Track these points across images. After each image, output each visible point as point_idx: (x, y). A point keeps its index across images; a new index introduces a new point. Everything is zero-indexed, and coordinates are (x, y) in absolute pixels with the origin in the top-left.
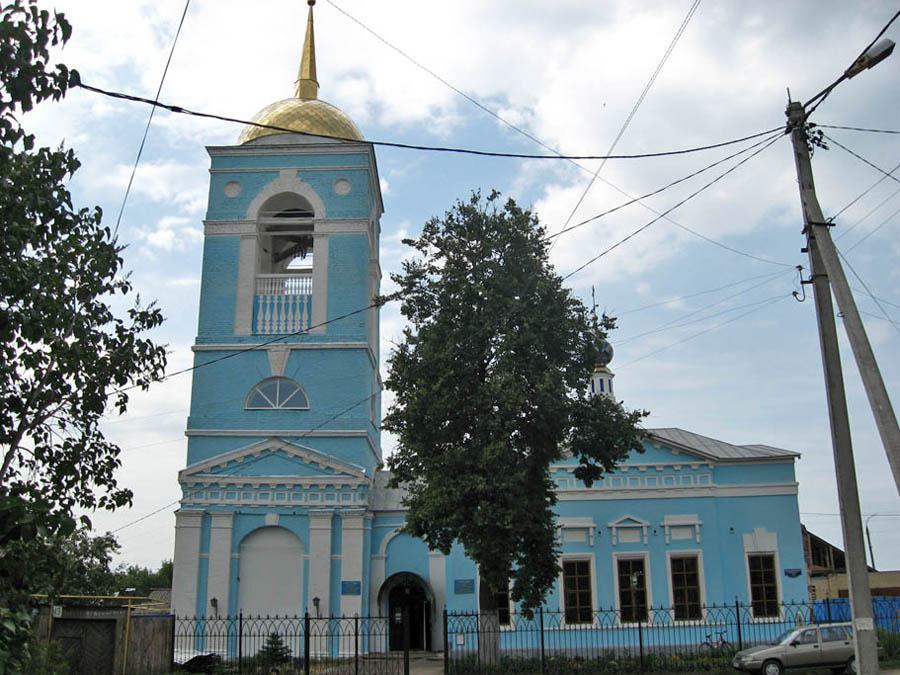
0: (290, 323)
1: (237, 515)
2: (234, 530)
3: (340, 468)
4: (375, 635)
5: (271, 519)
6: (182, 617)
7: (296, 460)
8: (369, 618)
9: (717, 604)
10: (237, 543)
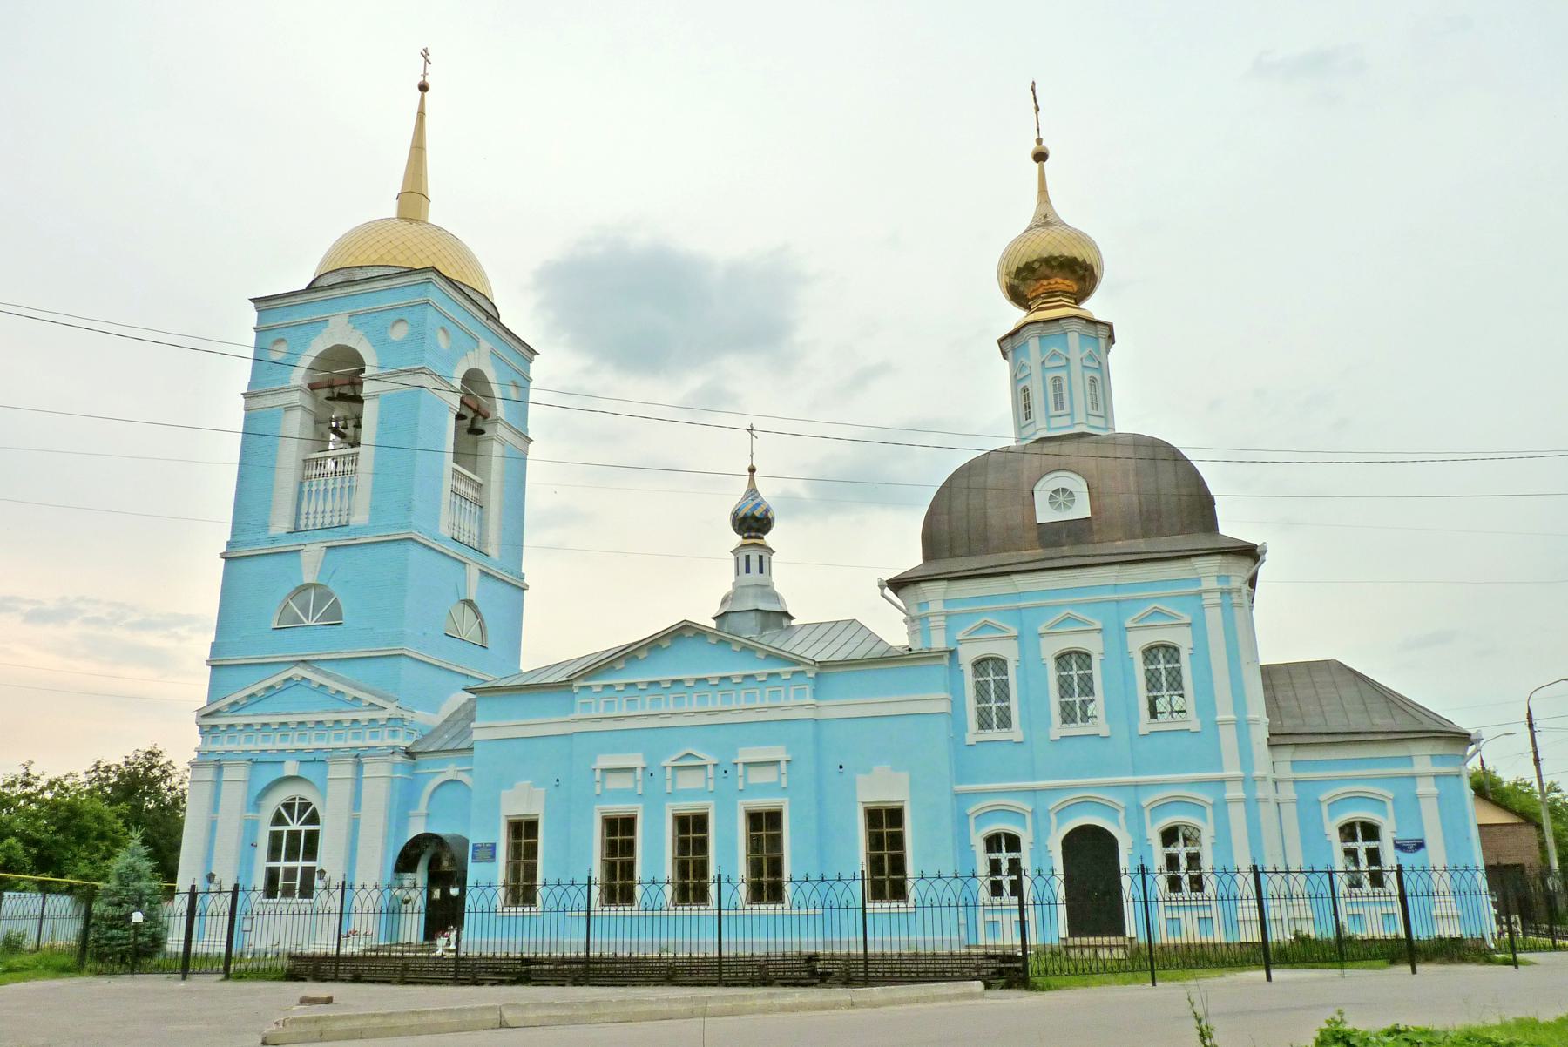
0: (319, 515)
1: (254, 762)
2: (250, 783)
3: (367, 698)
4: (406, 913)
5: (290, 768)
7: (321, 689)
9: (944, 874)
10: (253, 800)
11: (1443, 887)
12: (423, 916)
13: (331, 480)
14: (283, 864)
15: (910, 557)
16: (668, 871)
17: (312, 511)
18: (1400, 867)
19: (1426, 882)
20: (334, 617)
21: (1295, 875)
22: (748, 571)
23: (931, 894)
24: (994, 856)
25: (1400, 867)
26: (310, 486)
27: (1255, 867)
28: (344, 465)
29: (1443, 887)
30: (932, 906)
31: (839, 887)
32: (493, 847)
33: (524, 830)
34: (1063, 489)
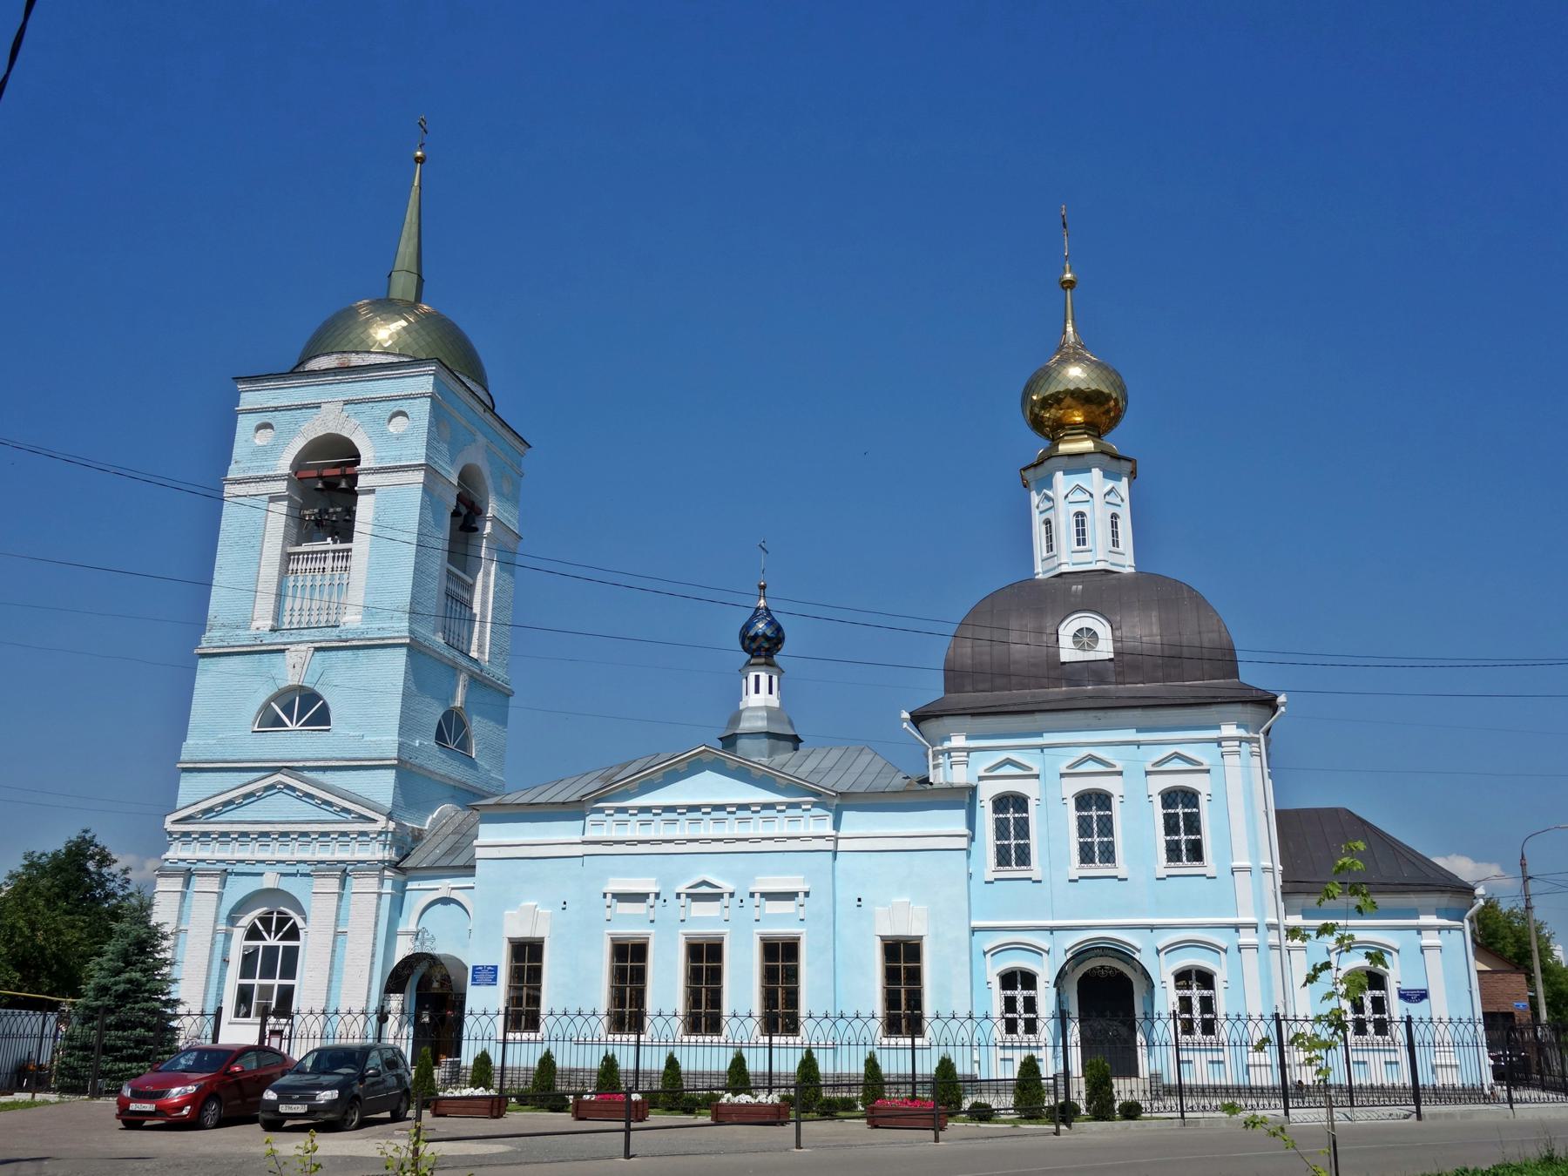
0: (306, 613)
5: (270, 880)
6: (304, 1010)
8: (202, 1015)
11: (1448, 1038)
12: (410, 1041)
13: (319, 577)
14: (257, 982)
15: (933, 690)
16: (755, 1004)
17: (297, 607)
18: (1409, 1017)
19: (1472, 1032)
20: (322, 718)
21: (1397, 1023)
22: (757, 691)
23: (850, 1032)
24: (1009, 993)
25: (1409, 1017)
26: (296, 580)
27: (1277, 1015)
28: (334, 561)
29: (1448, 1038)
30: (865, 1044)
31: (857, 1024)
32: (495, 969)
33: (527, 955)
34: (1087, 628)
